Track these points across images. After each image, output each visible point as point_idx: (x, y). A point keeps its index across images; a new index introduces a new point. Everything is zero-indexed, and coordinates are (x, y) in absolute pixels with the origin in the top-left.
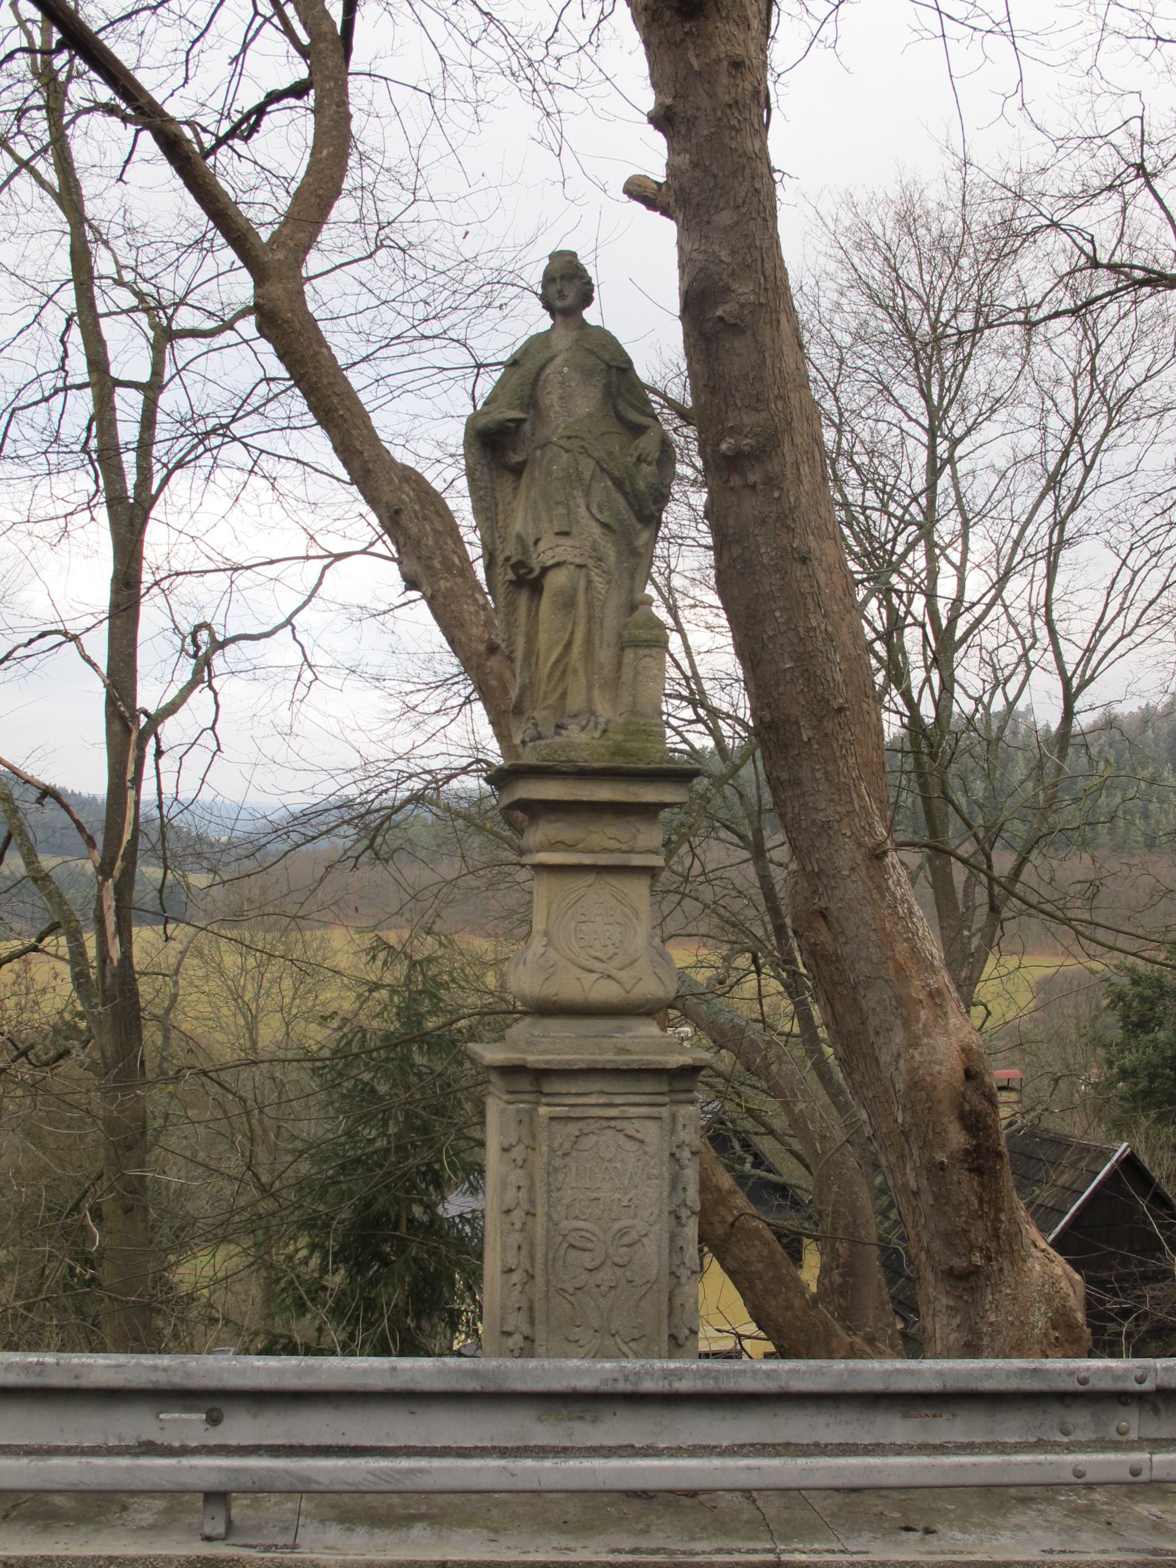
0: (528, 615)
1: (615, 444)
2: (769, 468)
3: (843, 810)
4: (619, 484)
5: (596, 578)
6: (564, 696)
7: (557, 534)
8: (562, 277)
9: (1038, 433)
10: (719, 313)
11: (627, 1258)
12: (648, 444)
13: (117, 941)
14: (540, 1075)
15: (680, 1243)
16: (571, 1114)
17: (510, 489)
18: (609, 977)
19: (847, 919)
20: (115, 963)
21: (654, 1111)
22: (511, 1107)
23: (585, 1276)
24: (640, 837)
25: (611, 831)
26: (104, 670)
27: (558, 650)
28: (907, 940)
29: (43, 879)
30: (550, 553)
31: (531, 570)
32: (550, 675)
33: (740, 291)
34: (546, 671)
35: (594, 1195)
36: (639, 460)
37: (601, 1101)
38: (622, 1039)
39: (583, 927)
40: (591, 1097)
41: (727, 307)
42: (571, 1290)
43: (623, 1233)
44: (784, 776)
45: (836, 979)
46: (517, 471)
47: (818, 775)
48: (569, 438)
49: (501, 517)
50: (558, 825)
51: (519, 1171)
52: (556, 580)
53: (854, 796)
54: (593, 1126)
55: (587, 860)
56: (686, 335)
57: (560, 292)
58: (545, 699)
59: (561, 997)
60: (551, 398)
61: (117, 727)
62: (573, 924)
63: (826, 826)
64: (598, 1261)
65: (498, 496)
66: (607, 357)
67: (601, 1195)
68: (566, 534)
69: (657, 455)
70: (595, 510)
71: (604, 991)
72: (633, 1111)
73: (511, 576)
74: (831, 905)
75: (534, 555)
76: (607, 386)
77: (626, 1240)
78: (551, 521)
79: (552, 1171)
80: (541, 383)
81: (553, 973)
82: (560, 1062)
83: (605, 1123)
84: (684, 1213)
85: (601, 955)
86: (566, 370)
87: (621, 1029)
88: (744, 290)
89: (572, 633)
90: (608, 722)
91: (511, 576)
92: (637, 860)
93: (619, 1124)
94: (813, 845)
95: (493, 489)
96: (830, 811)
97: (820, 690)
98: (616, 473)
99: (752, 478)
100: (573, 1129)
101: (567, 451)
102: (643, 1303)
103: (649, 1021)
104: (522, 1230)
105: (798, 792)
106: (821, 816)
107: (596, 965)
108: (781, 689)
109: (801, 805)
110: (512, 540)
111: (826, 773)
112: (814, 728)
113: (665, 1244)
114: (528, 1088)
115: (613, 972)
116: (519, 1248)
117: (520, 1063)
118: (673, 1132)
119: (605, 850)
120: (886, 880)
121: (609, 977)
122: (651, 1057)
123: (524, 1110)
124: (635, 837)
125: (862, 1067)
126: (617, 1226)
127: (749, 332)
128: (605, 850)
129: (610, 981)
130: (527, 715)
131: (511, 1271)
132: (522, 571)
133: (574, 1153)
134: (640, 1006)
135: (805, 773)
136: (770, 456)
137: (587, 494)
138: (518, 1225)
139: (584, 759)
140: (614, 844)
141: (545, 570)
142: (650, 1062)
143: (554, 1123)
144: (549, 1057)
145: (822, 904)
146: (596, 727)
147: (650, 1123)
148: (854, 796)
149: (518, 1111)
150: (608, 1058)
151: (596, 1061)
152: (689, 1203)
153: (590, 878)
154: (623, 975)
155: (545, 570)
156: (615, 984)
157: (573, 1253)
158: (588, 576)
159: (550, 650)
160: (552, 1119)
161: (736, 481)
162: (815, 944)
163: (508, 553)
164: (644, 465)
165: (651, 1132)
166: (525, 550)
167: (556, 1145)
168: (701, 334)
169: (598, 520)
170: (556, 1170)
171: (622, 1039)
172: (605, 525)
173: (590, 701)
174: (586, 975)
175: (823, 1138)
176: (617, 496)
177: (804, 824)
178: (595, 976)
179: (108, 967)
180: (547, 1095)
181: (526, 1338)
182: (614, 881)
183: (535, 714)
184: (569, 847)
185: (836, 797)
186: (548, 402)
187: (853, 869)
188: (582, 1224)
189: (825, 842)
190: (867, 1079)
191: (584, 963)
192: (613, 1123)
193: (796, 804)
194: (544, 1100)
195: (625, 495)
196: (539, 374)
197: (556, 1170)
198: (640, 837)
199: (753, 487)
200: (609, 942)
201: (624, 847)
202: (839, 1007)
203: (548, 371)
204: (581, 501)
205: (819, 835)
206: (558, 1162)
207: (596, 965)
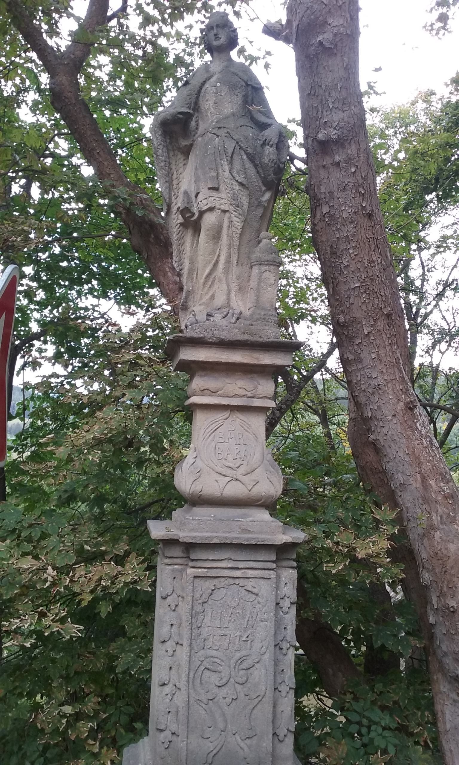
0: (192, 246)
1: (250, 133)
2: (349, 152)
4: (252, 158)
5: (234, 219)
6: (213, 297)
7: (210, 189)
8: (217, 26)
10: (320, 38)
11: (244, 679)
12: (270, 134)
14: (189, 547)
15: (282, 667)
16: (209, 575)
17: (181, 165)
18: (237, 479)
21: (266, 573)
22: (168, 567)
23: (216, 690)
27: (210, 266)
28: (429, 461)
30: (205, 202)
31: (193, 214)
32: (205, 284)
33: (334, 24)
34: (202, 281)
35: (223, 632)
36: (264, 144)
37: (229, 566)
39: (219, 445)
40: (224, 561)
41: (325, 36)
42: (205, 701)
43: (241, 660)
44: (351, 357)
46: (187, 152)
48: (219, 128)
49: (175, 182)
50: (206, 378)
51: (172, 613)
52: (209, 220)
54: (223, 582)
55: (225, 401)
56: (297, 60)
57: (215, 35)
58: (201, 299)
59: (204, 492)
60: (208, 104)
62: (213, 444)
64: (225, 680)
65: (173, 167)
66: (245, 78)
67: (227, 632)
68: (216, 189)
69: (276, 141)
70: (235, 174)
71: (233, 490)
72: (250, 573)
73: (181, 220)
75: (195, 205)
76: (246, 96)
77: (245, 665)
78: (206, 181)
79: (193, 615)
80: (202, 94)
82: (202, 538)
83: (231, 581)
84: (285, 645)
86: (218, 84)
87: (245, 516)
88: (335, 21)
89: (219, 256)
90: (241, 313)
91: (181, 220)
92: (257, 403)
93: (242, 582)
95: (170, 164)
96: (380, 379)
97: (376, 302)
98: (250, 151)
99: (337, 158)
100: (209, 584)
101: (218, 136)
102: (255, 711)
104: (172, 656)
105: (360, 367)
106: (375, 382)
107: (228, 472)
108: (351, 301)
109: (361, 375)
110: (181, 195)
111: (378, 355)
112: (372, 326)
113: (271, 669)
114: (181, 555)
115: (240, 477)
116: (171, 668)
117: (175, 538)
118: (277, 588)
119: (236, 396)
120: (416, 423)
121: (237, 479)
122: (263, 536)
123: (177, 570)
126: (238, 655)
127: (339, 55)
128: (236, 396)
130: (190, 310)
131: (164, 684)
132: (188, 215)
133: (210, 602)
134: (259, 500)
135: (364, 355)
136: (350, 143)
137: (231, 162)
138: (170, 652)
139: (224, 335)
140: (242, 392)
141: (202, 213)
143: (197, 580)
144: (195, 534)
146: (233, 316)
147: (262, 582)
149: (173, 571)
150: (235, 535)
151: (226, 538)
152: (289, 639)
153: (226, 414)
155: (202, 213)
157: (207, 673)
158: (230, 218)
159: (205, 266)
160: (195, 577)
161: (327, 161)
163: (179, 205)
164: (268, 147)
165: (265, 589)
166: (189, 202)
167: (197, 595)
168: (307, 57)
169: (237, 181)
170: (197, 613)
172: (241, 184)
173: (228, 299)
176: (249, 165)
178: (228, 479)
180: (193, 560)
181: (173, 734)
183: (194, 309)
184: (213, 393)
186: (207, 107)
187: (395, 415)
188: (214, 653)
191: (220, 470)
192: (237, 581)
193: (359, 375)
194: (191, 564)
195: (256, 166)
196: (201, 88)
197: (197, 613)
198: (260, 387)
199: (338, 164)
201: (249, 394)
203: (207, 85)
204: (226, 168)
206: (198, 608)
207: (228, 472)
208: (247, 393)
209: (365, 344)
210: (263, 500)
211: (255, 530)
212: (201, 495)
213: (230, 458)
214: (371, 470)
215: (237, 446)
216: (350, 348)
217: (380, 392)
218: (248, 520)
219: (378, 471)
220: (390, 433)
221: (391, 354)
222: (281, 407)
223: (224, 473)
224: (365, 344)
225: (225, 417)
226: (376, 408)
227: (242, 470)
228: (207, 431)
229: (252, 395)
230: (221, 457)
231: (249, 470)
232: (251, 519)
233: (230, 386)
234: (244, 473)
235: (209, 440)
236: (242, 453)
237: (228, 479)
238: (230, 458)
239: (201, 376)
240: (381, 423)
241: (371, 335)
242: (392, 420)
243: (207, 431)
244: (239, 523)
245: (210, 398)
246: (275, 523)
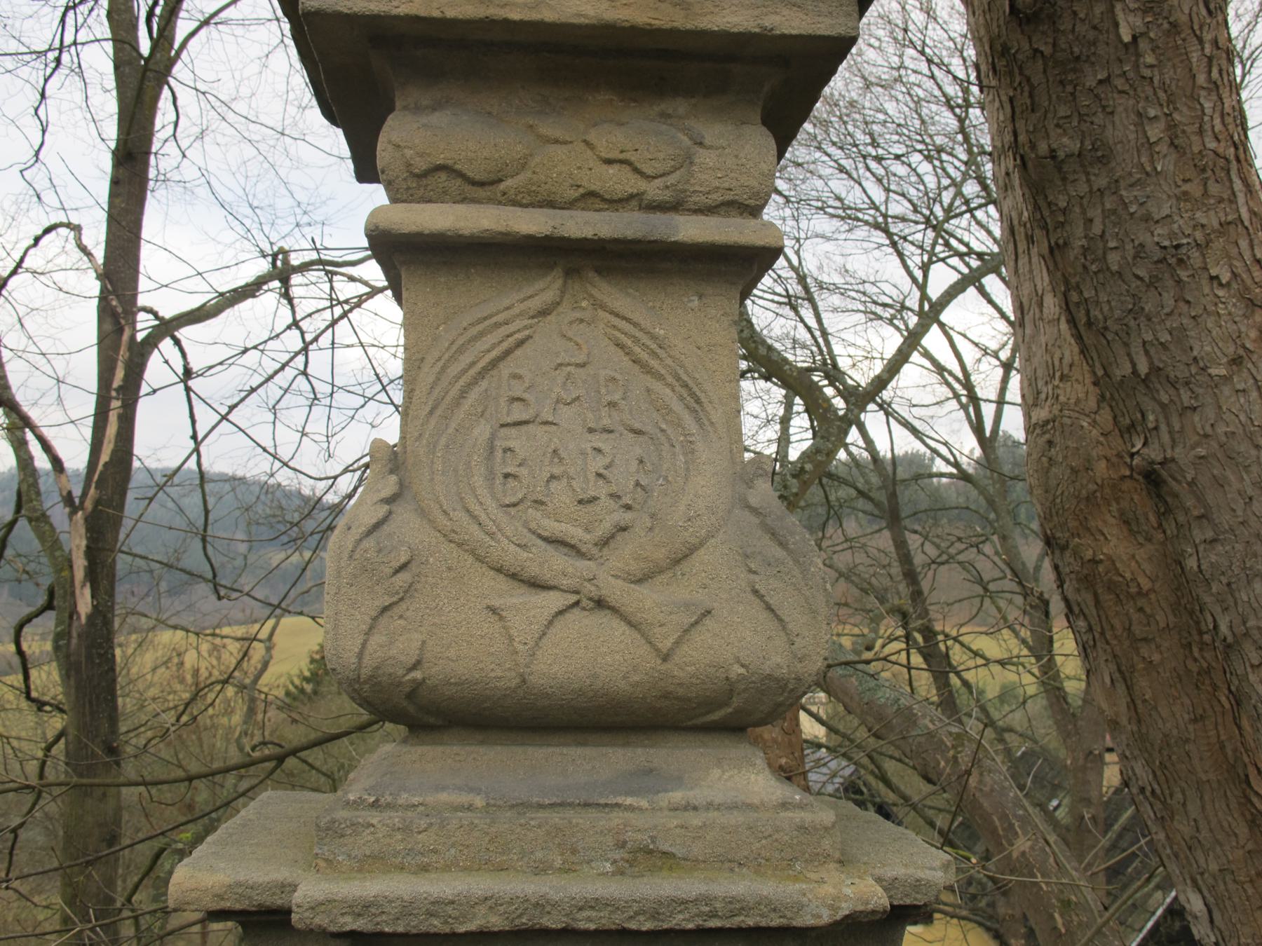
3: (1212, 220)
9: (842, 579)
13: (87, 591)
18: (600, 604)
19: (1220, 483)
20: (83, 619)
24: (705, 158)
25: (610, 139)
26: (100, 260)
29: (37, 519)
38: (647, 816)
39: (514, 439)
44: (1068, 144)
45: (1138, 630)
47: (1155, 132)
50: (439, 119)
53: (1238, 185)
61: (108, 327)
62: (482, 431)
63: (1172, 258)
71: (585, 654)
74: (1179, 453)
81: (408, 592)
82: (408, 908)
85: (574, 533)
87: (648, 781)
94: (1136, 312)
96: (1180, 223)
103: (737, 750)
105: (1102, 182)
107: (556, 564)
109: (1106, 214)
111: (1172, 127)
115: (615, 590)
119: (590, 198)
121: (600, 604)
124: (688, 160)
125: (1194, 809)
128: (590, 198)
129: (604, 618)
134: (711, 704)
135: (1120, 130)
140: (618, 181)
142: (738, 905)
145: (1154, 453)
148: (1238, 185)
151: (541, 905)
153: (545, 288)
154: (646, 600)
156: (620, 628)
162: (1095, 562)
171: (647, 816)
174: (518, 598)
175: (1066, 904)
177: (1114, 260)
178: (555, 601)
179: (75, 624)
182: (620, 298)
184: (480, 186)
185: (1194, 189)
187: (1236, 361)
189: (1169, 300)
190: (1204, 834)
191: (512, 556)
193: (1095, 213)
198: (705, 158)
200: (602, 490)
201: (654, 190)
202: (1143, 684)
205: (1153, 283)
207: (556, 564)
208: (642, 185)
209: (1119, 83)
210: (736, 702)
211: (697, 850)
212: (418, 684)
213: (561, 495)
214: (1111, 587)
215: (598, 441)
216: (1063, 111)
217: (1184, 274)
218: (664, 799)
219: (1133, 590)
220: (1221, 429)
221: (1217, 121)
222: (802, 469)
223: (533, 570)
224: (1119, 83)
225: (536, 304)
226: (1165, 337)
227: (624, 555)
228: (454, 370)
229: (666, 196)
230: (515, 492)
231: (661, 555)
232: (677, 796)
233: (559, 152)
234: (635, 568)
235: (460, 414)
236: (623, 479)
237: (555, 601)
238: (561, 495)
239: (418, 109)
240: (1185, 396)
241: (1143, 45)
242: (1227, 379)
243: (454, 370)
244: (616, 818)
245: (461, 208)
246: (798, 816)
